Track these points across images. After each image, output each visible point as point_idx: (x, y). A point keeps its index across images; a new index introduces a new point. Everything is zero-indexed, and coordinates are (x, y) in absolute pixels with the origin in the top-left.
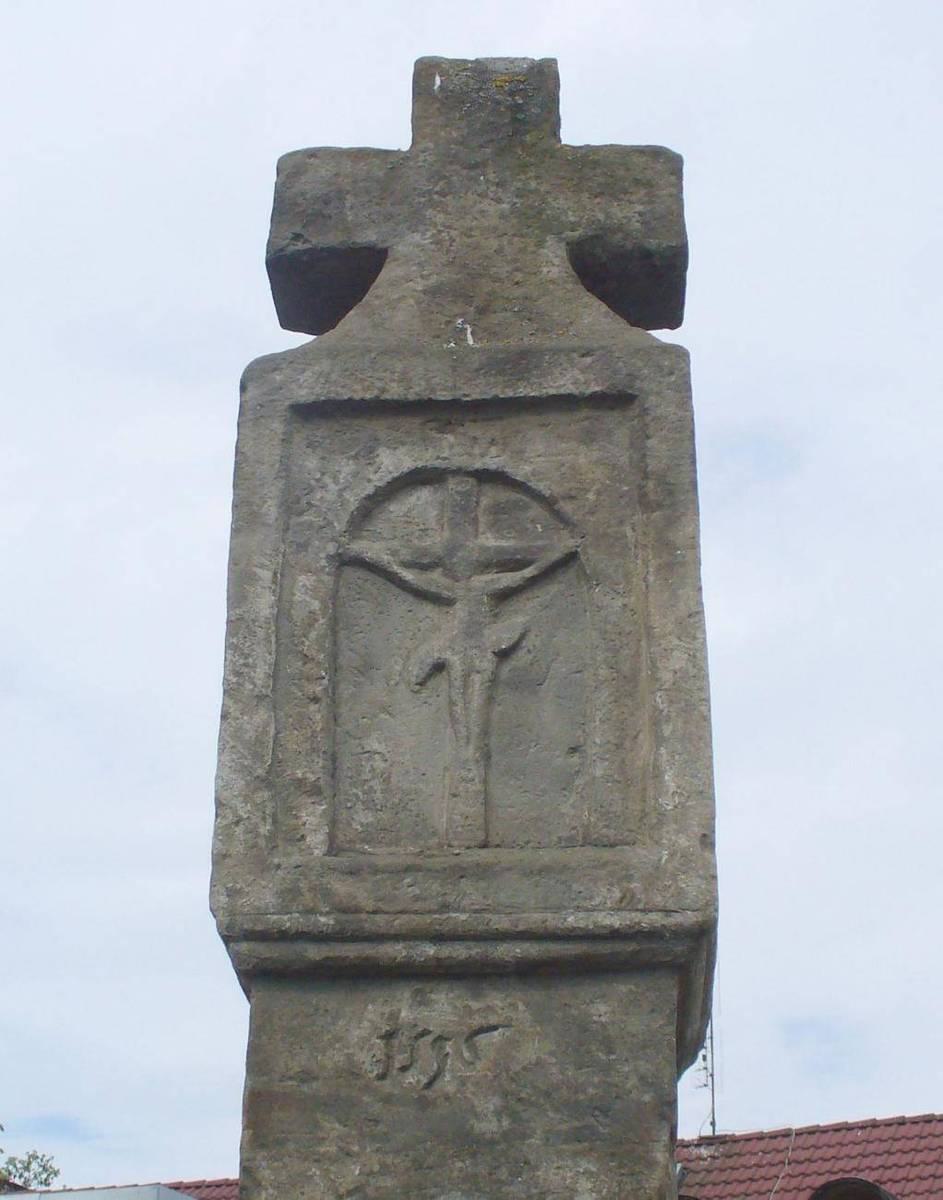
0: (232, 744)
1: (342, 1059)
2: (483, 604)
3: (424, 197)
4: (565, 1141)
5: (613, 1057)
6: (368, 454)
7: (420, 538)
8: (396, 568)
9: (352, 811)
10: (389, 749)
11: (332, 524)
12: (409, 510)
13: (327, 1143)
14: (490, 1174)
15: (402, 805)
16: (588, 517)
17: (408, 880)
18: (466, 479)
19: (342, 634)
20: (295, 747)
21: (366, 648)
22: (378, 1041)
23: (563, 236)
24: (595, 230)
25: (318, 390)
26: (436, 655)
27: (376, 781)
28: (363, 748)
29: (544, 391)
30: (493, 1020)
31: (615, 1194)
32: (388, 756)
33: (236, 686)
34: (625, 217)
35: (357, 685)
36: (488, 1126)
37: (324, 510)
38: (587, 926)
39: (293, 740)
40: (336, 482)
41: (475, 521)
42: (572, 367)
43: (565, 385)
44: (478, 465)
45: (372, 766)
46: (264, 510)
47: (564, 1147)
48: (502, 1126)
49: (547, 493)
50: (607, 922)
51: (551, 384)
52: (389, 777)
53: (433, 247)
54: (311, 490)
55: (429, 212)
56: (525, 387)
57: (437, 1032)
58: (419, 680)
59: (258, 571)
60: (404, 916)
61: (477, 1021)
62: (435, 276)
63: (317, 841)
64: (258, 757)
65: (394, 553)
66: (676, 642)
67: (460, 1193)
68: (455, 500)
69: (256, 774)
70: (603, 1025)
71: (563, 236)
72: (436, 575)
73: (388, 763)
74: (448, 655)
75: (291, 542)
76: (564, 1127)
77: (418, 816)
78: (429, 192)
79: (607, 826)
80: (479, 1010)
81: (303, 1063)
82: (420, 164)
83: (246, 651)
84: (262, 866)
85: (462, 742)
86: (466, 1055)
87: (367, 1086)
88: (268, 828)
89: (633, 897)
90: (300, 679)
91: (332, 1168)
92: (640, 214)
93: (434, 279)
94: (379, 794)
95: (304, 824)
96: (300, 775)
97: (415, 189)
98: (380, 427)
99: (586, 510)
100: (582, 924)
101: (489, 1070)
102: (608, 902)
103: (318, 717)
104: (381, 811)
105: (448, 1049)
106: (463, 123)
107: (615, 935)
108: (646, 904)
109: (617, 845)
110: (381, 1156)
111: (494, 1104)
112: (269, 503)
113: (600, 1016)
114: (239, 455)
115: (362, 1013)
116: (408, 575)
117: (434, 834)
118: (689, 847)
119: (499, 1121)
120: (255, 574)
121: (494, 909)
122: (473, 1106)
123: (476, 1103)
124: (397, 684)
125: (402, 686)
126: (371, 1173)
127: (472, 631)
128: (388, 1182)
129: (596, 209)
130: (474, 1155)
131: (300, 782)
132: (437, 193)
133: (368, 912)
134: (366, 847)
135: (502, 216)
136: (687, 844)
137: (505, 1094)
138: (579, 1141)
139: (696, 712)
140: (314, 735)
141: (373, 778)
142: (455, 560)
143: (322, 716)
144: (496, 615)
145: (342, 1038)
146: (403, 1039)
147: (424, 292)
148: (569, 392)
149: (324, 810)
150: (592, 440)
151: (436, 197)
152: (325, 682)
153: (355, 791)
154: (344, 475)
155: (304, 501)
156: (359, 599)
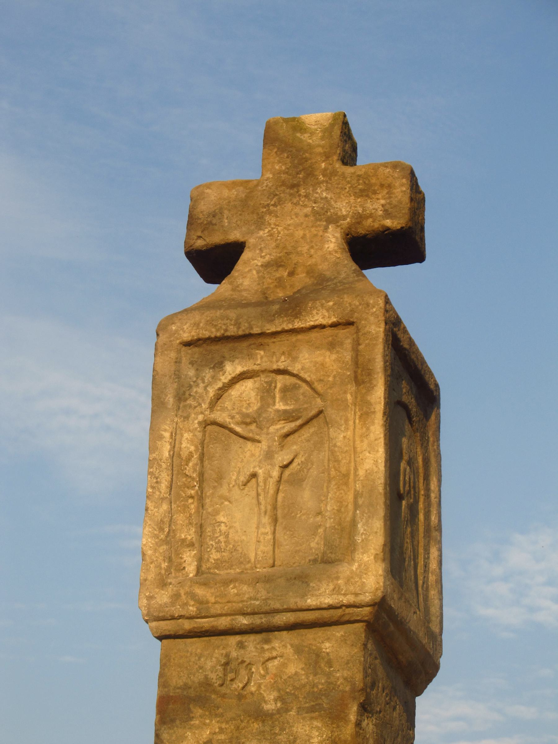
0: (149, 523)
1: (202, 677)
2: (275, 441)
3: (265, 208)
4: (307, 713)
5: (332, 669)
6: (219, 366)
7: (247, 408)
8: (232, 426)
9: (210, 553)
10: (228, 520)
11: (201, 405)
12: (241, 394)
13: (194, 719)
14: (271, 730)
15: (234, 548)
16: (329, 391)
17: (231, 586)
18: (269, 374)
19: (206, 463)
20: (181, 522)
21: (219, 468)
22: (220, 668)
23: (339, 224)
24: (357, 219)
25: (193, 333)
26: (251, 470)
27: (222, 537)
28: (216, 521)
29: (308, 324)
30: (274, 654)
31: (329, 737)
32: (228, 524)
33: (151, 494)
34: (374, 209)
35: (215, 487)
36: (270, 706)
37: (197, 397)
38: (317, 603)
39: (180, 519)
40: (204, 382)
41: (274, 398)
42: (322, 308)
43: (318, 319)
44: (275, 367)
45: (220, 529)
46: (166, 400)
47: (306, 715)
48: (277, 706)
49: (308, 379)
50: (326, 601)
51: (311, 319)
52: (228, 534)
53: (269, 238)
54: (190, 387)
55: (267, 218)
56: (298, 322)
57: (248, 661)
58: (244, 484)
59: (163, 433)
60: (230, 604)
61: (267, 655)
62: (268, 256)
63: (191, 569)
64: (161, 529)
65: (233, 417)
66: (368, 454)
67: (256, 740)
68: (264, 386)
69: (160, 538)
70: (328, 654)
71: (339, 224)
72: (253, 427)
73: (228, 527)
74: (257, 469)
75: (181, 416)
76: (307, 705)
77: (241, 553)
78: (268, 205)
79: (331, 553)
80: (268, 649)
81: (184, 681)
82: (264, 188)
83: (157, 475)
84: (163, 584)
85: (263, 515)
86: (262, 672)
87: (214, 690)
88: (166, 564)
89: (339, 588)
90: (184, 488)
91: (196, 732)
92: (383, 206)
93: (267, 258)
94: (223, 544)
95: (185, 561)
96: (183, 537)
97: (260, 204)
98: (224, 349)
99: (328, 386)
100: (314, 603)
101: (272, 679)
102: (327, 591)
103: (192, 506)
104: (224, 552)
105: (253, 670)
106: (288, 160)
107: (331, 607)
108: (346, 591)
109: (336, 562)
110: (220, 724)
111: (274, 696)
112: (168, 397)
113: (326, 649)
114: (155, 371)
115: (213, 654)
116: (238, 429)
117: (249, 562)
118: (368, 561)
119: (275, 703)
120: (162, 435)
121: (272, 598)
122: (264, 697)
123: (265, 695)
124: (234, 486)
125: (236, 487)
126: (215, 733)
127: (269, 455)
128: (222, 737)
129: (358, 206)
130: (263, 721)
131: (184, 540)
132: (272, 205)
133: (212, 603)
134: (216, 570)
135: (306, 216)
136: (368, 559)
137: (279, 690)
138: (314, 712)
139: (376, 491)
140: (191, 515)
141: (220, 535)
142: (261, 419)
143: (195, 506)
144: (283, 446)
145: (203, 667)
146: (233, 665)
147: (262, 266)
148: (320, 323)
149: (195, 554)
150: (333, 348)
151: (271, 207)
152: (197, 488)
153: (211, 542)
154: (207, 378)
155: (187, 393)
156: (216, 443)
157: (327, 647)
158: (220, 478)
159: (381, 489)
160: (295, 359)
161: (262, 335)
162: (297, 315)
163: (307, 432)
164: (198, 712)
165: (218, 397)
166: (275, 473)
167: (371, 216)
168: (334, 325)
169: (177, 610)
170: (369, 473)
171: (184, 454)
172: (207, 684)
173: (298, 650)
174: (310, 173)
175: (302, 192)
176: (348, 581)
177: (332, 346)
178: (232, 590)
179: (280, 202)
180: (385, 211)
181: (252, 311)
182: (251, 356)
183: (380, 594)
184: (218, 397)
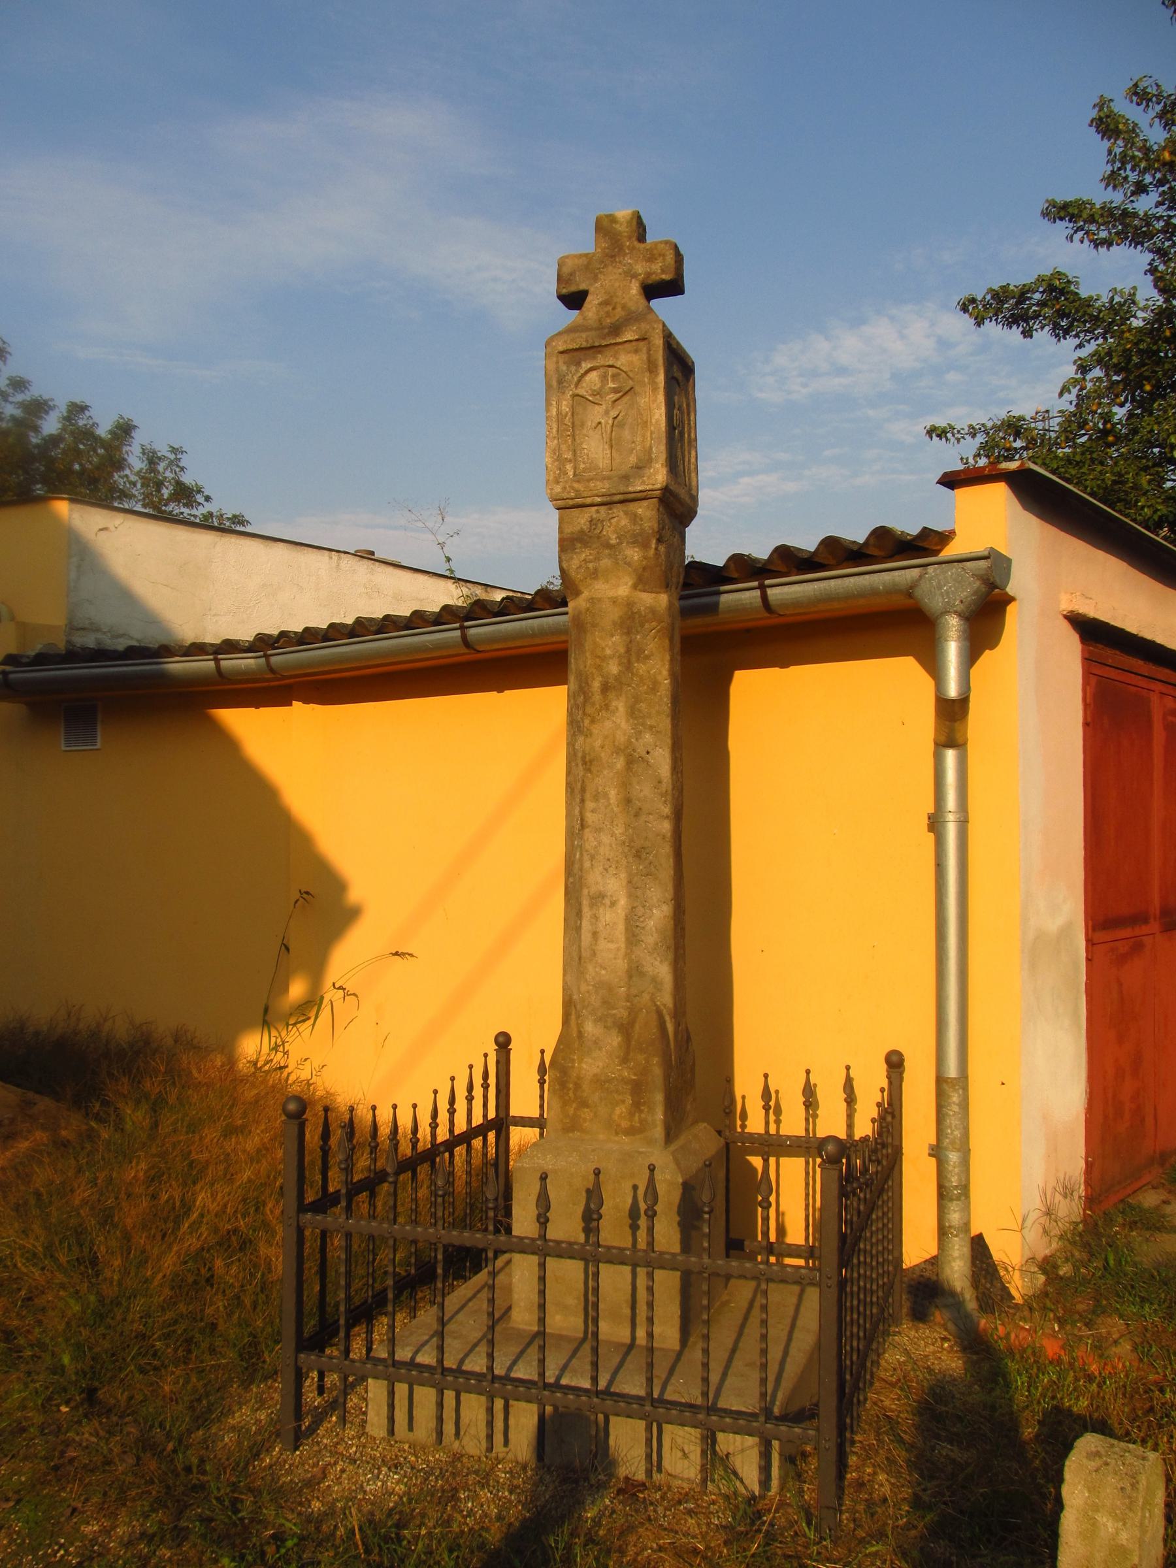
36: (613, 542)
39: (564, 447)
61: (611, 516)
63: (571, 474)
72: (598, 397)
107: (641, 491)
127: (607, 412)
157: (640, 511)
158: (583, 425)
161: (600, 346)
163: (626, 399)
166: (610, 422)
167: (654, 273)
168: (637, 340)
169: (565, 495)
170: (657, 421)
171: (563, 413)
174: (621, 248)
175: (617, 260)
177: (636, 351)
179: (606, 266)
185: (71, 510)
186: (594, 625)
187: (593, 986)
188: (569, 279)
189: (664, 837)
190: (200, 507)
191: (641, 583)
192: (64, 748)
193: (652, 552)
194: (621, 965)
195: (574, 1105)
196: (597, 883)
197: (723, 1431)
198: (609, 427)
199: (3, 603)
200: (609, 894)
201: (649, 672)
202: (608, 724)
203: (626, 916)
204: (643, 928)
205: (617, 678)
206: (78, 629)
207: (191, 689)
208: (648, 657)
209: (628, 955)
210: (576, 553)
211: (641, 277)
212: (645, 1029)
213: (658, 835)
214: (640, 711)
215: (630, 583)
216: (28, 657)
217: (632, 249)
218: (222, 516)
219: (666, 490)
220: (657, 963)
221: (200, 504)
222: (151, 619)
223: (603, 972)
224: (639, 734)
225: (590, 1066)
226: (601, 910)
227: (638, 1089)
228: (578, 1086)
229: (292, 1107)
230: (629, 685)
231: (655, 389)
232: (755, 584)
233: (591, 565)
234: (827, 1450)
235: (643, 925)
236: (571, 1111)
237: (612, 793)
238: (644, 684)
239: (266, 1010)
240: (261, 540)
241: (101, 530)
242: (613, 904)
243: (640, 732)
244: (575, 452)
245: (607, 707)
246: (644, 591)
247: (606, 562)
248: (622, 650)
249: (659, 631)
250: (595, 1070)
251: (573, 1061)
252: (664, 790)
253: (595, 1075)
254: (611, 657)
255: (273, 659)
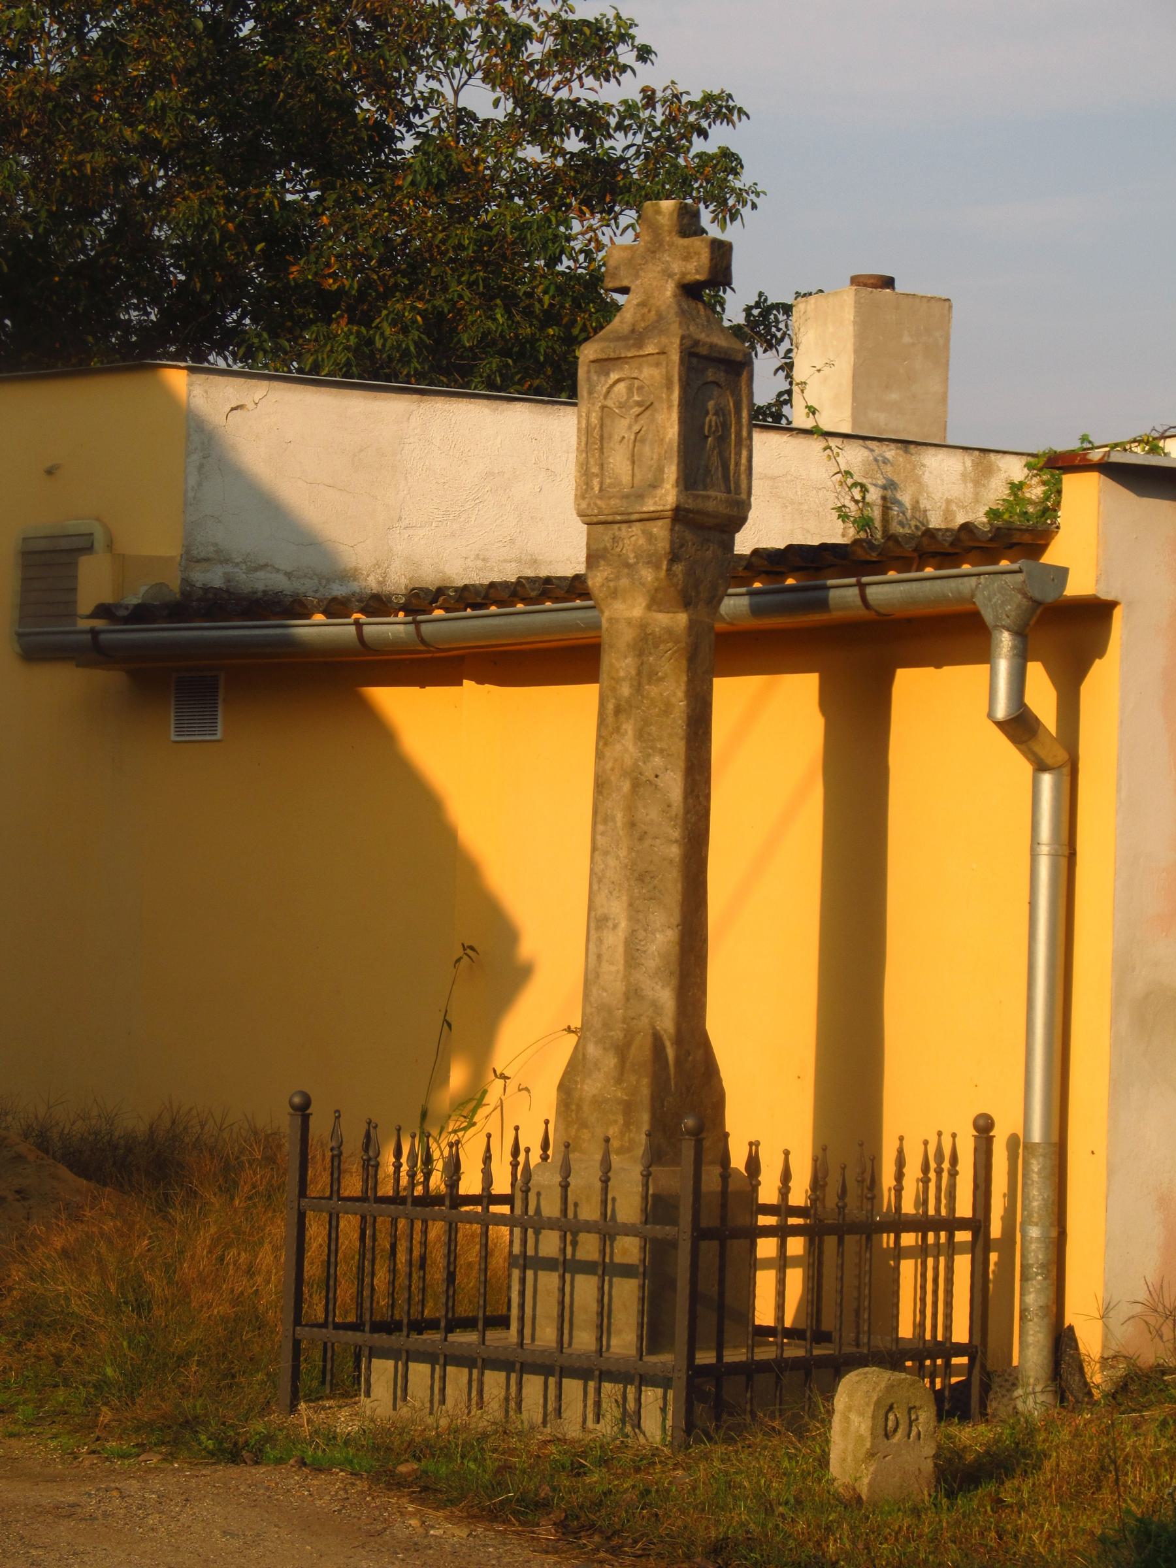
6: (607, 374)
36: (631, 561)
39: (592, 461)
61: (631, 534)
63: (597, 489)
72: (624, 410)
107: (653, 512)
127: (630, 427)
157: (655, 530)
158: (610, 437)
159: (676, 449)
160: (641, 372)
161: (626, 357)
162: (309, 618)
163: (648, 413)
164: (602, 563)
165: (608, 391)
166: (632, 437)
167: (689, 273)
168: (658, 353)
169: (589, 512)
170: (671, 440)
171: (593, 425)
172: (605, 549)
173: (643, 532)
174: (661, 245)
175: (657, 256)
176: (660, 499)
177: (658, 365)
178: (612, 502)
179: (646, 262)
180: (696, 270)
181: (621, 344)
182: (622, 369)
183: (674, 505)
184: (608, 391)
185: (190, 384)
186: (611, 646)
187: (596, 1008)
188: (614, 274)
189: (671, 862)
190: (627, 77)
191: (655, 603)
192: (174, 738)
193: (663, 574)
194: (619, 987)
195: (575, 1126)
196: (602, 906)
197: (461, 1222)
198: (631, 441)
199: (98, 519)
200: (612, 916)
201: (661, 694)
202: (618, 747)
203: (626, 939)
204: (645, 952)
205: (628, 701)
206: (198, 561)
207: (344, 659)
208: (661, 679)
209: (626, 977)
210: (600, 571)
211: (676, 277)
212: (641, 1050)
213: (664, 859)
214: (649, 734)
215: (644, 604)
216: (127, 608)
217: (671, 244)
218: (677, 97)
219: (677, 510)
220: (658, 987)
221: (623, 69)
222: (308, 541)
223: (605, 994)
224: (647, 758)
225: (591, 1087)
226: (605, 931)
227: (628, 1108)
228: (579, 1107)
229: (297, 1100)
230: (638, 708)
231: (670, 407)
232: (853, 580)
233: (611, 584)
234: (679, 1378)
235: (645, 949)
236: (573, 1133)
237: (619, 816)
238: (656, 706)
239: (424, 1115)
240: (485, 402)
241: (233, 409)
242: (615, 927)
243: (649, 755)
244: (602, 465)
245: (617, 730)
246: (660, 611)
247: (624, 582)
248: (633, 672)
249: (676, 652)
250: (595, 1092)
251: (576, 1082)
252: (674, 813)
253: (594, 1096)
254: (623, 679)
255: (424, 627)
